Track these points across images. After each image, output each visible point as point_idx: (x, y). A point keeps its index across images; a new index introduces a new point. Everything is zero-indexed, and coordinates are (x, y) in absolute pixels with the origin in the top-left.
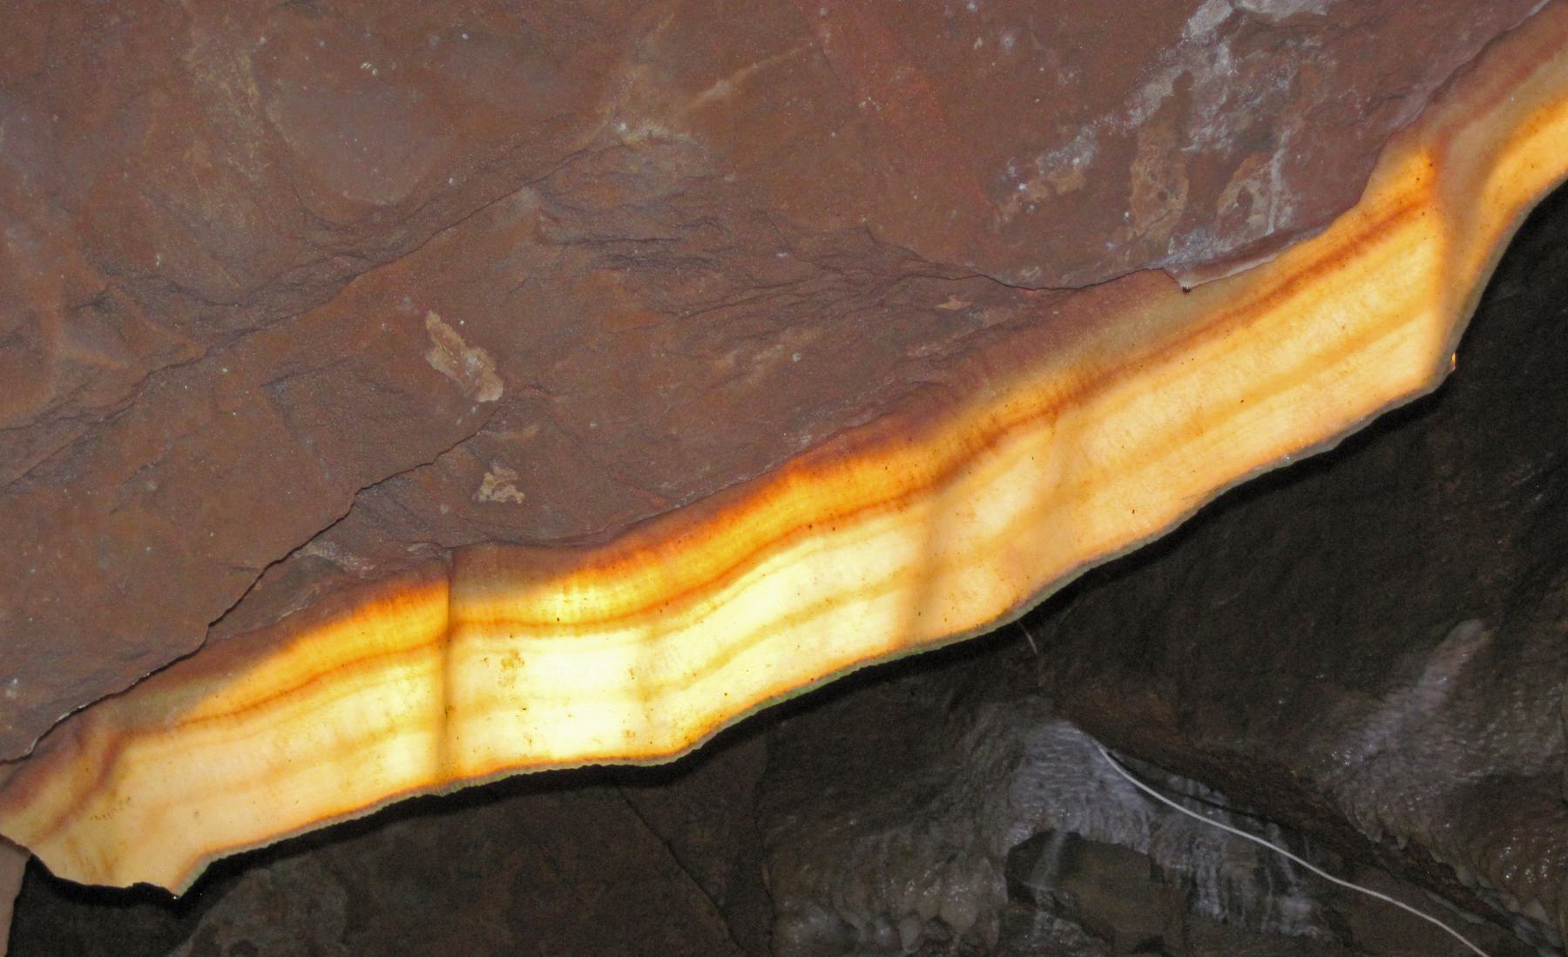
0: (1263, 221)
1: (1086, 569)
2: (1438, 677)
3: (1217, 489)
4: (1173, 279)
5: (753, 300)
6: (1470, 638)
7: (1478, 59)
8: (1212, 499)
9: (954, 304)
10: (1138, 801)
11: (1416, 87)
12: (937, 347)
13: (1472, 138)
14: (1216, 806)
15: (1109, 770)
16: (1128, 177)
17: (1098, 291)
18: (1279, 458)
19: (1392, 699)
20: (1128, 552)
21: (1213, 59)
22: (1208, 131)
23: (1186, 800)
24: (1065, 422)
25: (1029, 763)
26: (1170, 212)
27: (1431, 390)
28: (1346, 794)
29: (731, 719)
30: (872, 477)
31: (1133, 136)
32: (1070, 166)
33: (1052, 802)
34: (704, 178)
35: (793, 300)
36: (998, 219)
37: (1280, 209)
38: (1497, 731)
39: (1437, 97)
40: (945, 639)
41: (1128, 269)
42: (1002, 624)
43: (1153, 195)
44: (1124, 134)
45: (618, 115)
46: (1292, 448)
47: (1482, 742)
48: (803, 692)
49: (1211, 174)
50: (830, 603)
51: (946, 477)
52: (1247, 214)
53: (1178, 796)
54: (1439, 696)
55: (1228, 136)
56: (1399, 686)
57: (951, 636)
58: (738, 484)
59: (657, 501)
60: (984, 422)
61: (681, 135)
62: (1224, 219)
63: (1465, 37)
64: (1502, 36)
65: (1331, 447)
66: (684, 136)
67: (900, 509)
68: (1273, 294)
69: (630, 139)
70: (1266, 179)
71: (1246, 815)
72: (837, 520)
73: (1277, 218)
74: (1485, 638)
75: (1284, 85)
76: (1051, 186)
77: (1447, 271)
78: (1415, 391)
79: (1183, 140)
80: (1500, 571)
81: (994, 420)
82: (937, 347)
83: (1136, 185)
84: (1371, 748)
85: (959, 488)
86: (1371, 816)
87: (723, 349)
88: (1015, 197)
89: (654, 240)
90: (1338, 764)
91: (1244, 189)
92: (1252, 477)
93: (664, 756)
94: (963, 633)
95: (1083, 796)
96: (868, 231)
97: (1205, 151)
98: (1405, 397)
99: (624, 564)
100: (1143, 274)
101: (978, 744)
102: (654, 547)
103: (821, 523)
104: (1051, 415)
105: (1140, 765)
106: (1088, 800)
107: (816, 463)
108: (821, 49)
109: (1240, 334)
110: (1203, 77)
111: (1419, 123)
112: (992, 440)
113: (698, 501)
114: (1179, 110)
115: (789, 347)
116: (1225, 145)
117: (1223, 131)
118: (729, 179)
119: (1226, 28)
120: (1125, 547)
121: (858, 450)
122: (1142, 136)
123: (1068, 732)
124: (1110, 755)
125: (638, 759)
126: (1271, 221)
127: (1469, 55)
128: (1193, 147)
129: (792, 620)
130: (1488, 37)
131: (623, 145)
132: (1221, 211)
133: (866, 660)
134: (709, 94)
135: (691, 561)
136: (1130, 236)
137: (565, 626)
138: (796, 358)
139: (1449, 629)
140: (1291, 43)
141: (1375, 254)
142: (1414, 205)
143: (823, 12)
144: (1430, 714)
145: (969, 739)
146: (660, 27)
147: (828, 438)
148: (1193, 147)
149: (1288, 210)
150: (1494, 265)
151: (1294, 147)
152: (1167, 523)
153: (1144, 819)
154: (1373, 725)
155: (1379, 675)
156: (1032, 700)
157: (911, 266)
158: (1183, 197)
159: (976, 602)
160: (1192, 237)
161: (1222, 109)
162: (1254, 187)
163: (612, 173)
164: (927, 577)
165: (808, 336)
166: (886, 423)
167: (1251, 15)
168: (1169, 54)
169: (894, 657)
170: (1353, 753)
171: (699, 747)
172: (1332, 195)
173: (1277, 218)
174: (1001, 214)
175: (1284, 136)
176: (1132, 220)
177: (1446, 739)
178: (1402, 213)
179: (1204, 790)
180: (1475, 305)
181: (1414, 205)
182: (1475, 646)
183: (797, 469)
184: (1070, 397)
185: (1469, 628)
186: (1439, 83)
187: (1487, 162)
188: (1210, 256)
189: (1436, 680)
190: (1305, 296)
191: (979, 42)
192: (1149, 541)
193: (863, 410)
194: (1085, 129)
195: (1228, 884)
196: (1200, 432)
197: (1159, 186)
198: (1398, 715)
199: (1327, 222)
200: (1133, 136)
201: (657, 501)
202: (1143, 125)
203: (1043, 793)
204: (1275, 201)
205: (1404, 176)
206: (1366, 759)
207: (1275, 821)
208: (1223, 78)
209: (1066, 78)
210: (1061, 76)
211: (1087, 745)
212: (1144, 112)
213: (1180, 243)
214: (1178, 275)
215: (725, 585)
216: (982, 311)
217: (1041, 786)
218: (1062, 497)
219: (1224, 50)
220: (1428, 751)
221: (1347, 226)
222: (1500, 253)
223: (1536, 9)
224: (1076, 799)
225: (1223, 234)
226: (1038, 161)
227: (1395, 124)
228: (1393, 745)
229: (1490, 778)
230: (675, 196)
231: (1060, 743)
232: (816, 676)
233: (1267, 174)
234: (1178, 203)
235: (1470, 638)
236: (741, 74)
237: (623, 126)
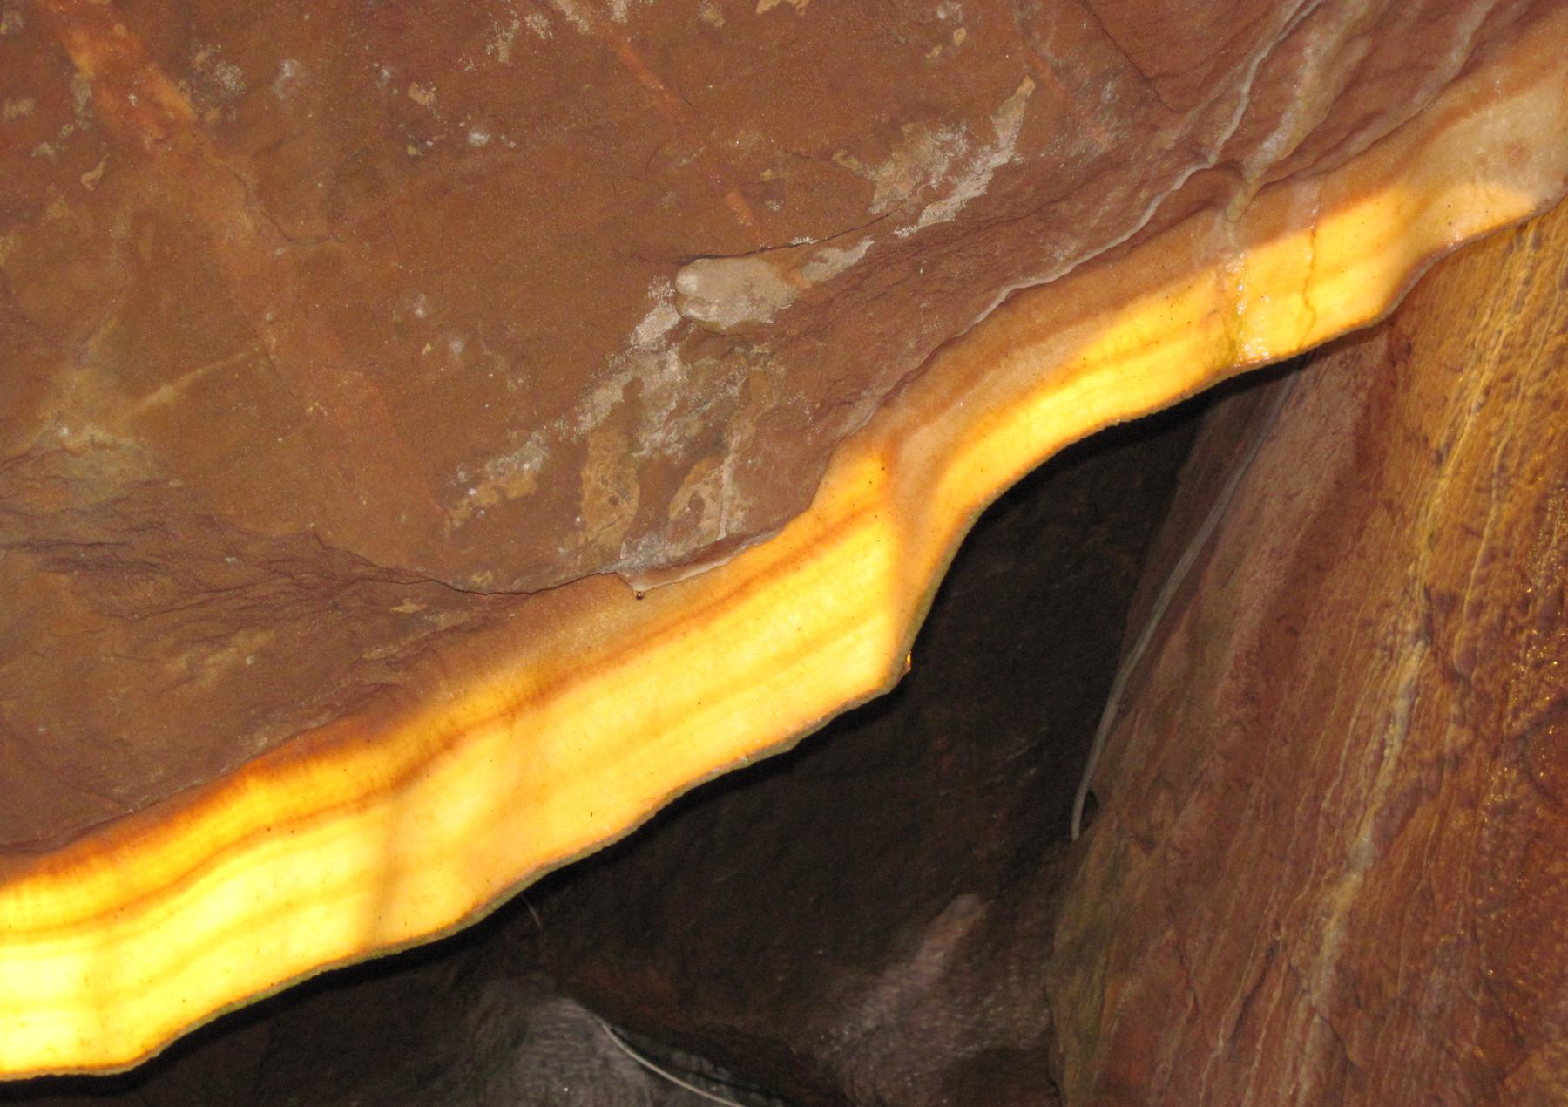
0: (720, 520)
1: (545, 872)
2: (934, 951)
3: (676, 790)
4: (626, 583)
5: (202, 604)
6: (964, 914)
7: (927, 363)
8: (669, 801)
9: (409, 607)
10: (642, 1078)
11: (864, 393)
12: (393, 649)
13: (922, 444)
14: (718, 1082)
15: (612, 1046)
16: (579, 481)
17: (554, 594)
18: (736, 760)
19: (890, 974)
20: (586, 855)
21: (662, 365)
22: (659, 436)
23: (690, 1076)
24: (524, 724)
25: (532, 1042)
26: (621, 517)
27: (886, 691)
28: (844, 1070)
29: (189, 1026)
30: (331, 779)
31: (584, 441)
32: (520, 471)
33: (555, 1080)
34: (148, 483)
35: (243, 604)
36: (448, 522)
37: (731, 514)
38: (995, 1005)
39: (887, 402)
40: (405, 943)
41: (579, 573)
42: (462, 927)
43: (604, 500)
44: (574, 439)
45: (60, 418)
46: (751, 750)
47: (977, 1017)
48: (262, 997)
49: (663, 479)
50: (289, 907)
51: (406, 779)
52: (698, 519)
53: (682, 1073)
54: (934, 971)
55: (678, 442)
56: (896, 961)
57: (411, 940)
58: (193, 788)
59: (110, 806)
60: (442, 724)
61: (124, 440)
62: (676, 524)
63: (912, 345)
64: (949, 343)
65: (788, 749)
66: (128, 441)
67: (360, 811)
68: (729, 596)
69: (73, 443)
70: (717, 482)
71: (751, 1090)
72: (295, 822)
73: (728, 523)
74: (980, 913)
75: (734, 391)
76: (502, 492)
77: (900, 571)
78: (872, 692)
79: (634, 445)
80: (995, 846)
81: (452, 722)
82: (393, 649)
83: (586, 492)
84: (869, 1024)
85: (123, 928)
86: (869, 1092)
87: (173, 652)
88: (465, 502)
89: (100, 544)
90: (838, 1040)
91: (695, 494)
92: (710, 779)
93: (120, 1065)
94: (423, 937)
95: (586, 1074)
96: (316, 536)
97: (656, 457)
98: (859, 698)
99: (78, 869)
100: (597, 577)
101: (482, 1021)
102: (108, 850)
103: (279, 825)
104: (509, 717)
105: (644, 1041)
106: (591, 1078)
107: (273, 764)
108: (267, 355)
109: (696, 636)
110: (653, 383)
111: (871, 427)
112: (450, 743)
113: (153, 804)
114: (629, 416)
115: (243, 650)
116: (676, 451)
117: (674, 436)
118: (175, 483)
119: (675, 335)
120: (583, 850)
121: (318, 749)
122: (592, 441)
123: (570, 1009)
124: (614, 1031)
125: (93, 1068)
126: (722, 526)
127: (916, 363)
128: (644, 453)
129: (252, 924)
130: (934, 344)
131: (64, 450)
132: (673, 516)
133: (327, 964)
134: (153, 399)
135: (148, 864)
136: (582, 541)
137: (17, 933)
138: (249, 661)
139: (946, 904)
140: (739, 350)
141: (831, 557)
142: (866, 509)
143: (268, 317)
144: (927, 989)
145: (473, 1017)
146: (103, 331)
147: (285, 741)
148: (644, 453)
149: (740, 514)
150: (945, 567)
151: (746, 451)
152: (625, 826)
153: (647, 1094)
154: (870, 1001)
155: (878, 951)
156: (536, 976)
157: (359, 570)
158: (635, 503)
159: (436, 905)
160: (645, 541)
161: (672, 414)
162: (705, 492)
163: (55, 477)
164: (387, 880)
165: (261, 639)
166: (345, 723)
167: (698, 322)
168: (619, 360)
169: (355, 961)
170: (853, 1029)
171: (156, 1055)
172: (782, 498)
173: (728, 523)
174: (452, 519)
175: (734, 443)
176: (584, 523)
177: (942, 1013)
178: (854, 517)
179: (707, 1066)
180: (926, 608)
181: (866, 509)
182: (970, 920)
183: (255, 771)
184: (527, 698)
185: (965, 902)
186: (888, 389)
187: (937, 466)
188: (662, 560)
189: (932, 956)
190: (761, 598)
191: (428, 348)
192: (608, 844)
193: (321, 711)
194: (535, 435)
195: (1354, 395)
196: (658, 734)
197: (611, 490)
198: (895, 990)
199: (781, 525)
200: (584, 441)
201: (110, 806)
202: (593, 431)
203: (544, 1071)
204: (726, 506)
205: (855, 480)
206: (864, 1034)
207: (779, 1097)
208: (673, 384)
209: (515, 383)
210: (509, 382)
211: (590, 1022)
212: (594, 418)
213: (632, 548)
214: (632, 580)
215: (181, 890)
216: (437, 613)
217: (544, 1064)
218: (520, 800)
219: (673, 356)
220: (925, 1026)
221: (800, 530)
222: (951, 556)
223: (982, 317)
224: (579, 1077)
225: (675, 538)
226: (488, 467)
227: (845, 429)
228: (891, 1020)
229: (986, 1052)
230: (117, 501)
231: (564, 1020)
232: (276, 981)
233: (718, 480)
234: (630, 507)
235: (964, 914)
236: (186, 380)
237: (65, 431)
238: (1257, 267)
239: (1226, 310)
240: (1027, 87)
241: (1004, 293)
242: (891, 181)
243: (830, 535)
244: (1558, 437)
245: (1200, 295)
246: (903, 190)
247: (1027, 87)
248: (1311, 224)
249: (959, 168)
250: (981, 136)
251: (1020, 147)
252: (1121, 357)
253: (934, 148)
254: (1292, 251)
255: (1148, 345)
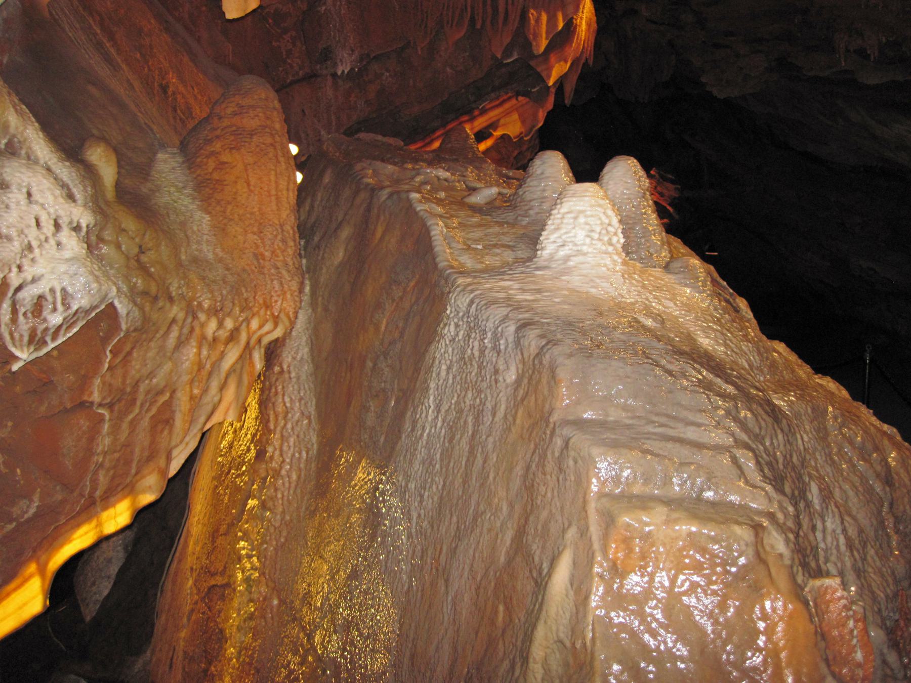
141: (27, 585)
178: (31, 576)
187: (46, 563)
190: (13, 596)
238: (105, 515)
239: (99, 525)
240: (39, 490)
241: (53, 527)
242: (16, 511)
243: (27, 580)
244: (453, 406)
245: (94, 523)
246: (19, 512)
247: (39, 490)
248: (114, 505)
249: (28, 507)
250: (31, 501)
251: (40, 501)
252: (81, 536)
253: (24, 503)
254: (111, 512)
255: (86, 533)
